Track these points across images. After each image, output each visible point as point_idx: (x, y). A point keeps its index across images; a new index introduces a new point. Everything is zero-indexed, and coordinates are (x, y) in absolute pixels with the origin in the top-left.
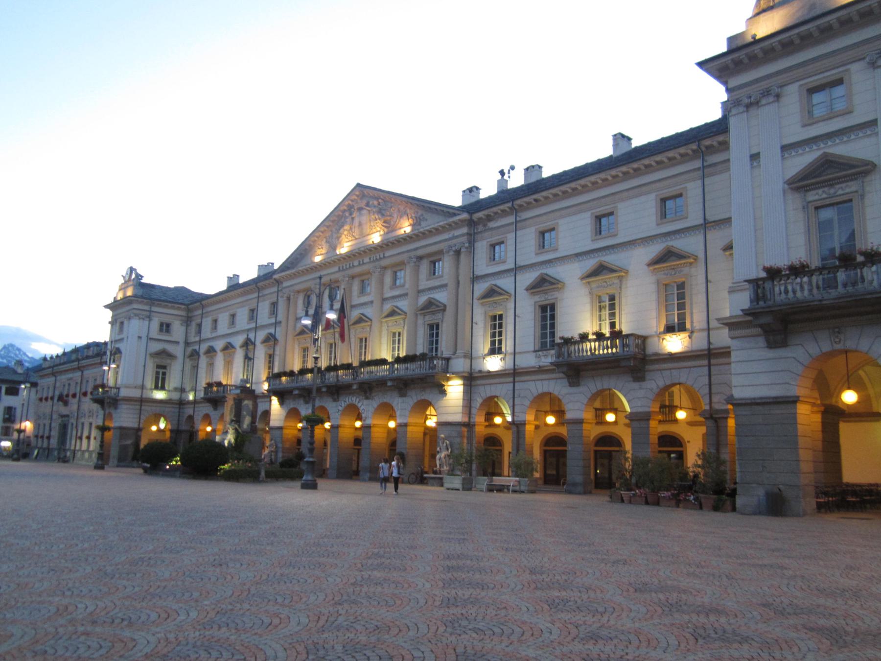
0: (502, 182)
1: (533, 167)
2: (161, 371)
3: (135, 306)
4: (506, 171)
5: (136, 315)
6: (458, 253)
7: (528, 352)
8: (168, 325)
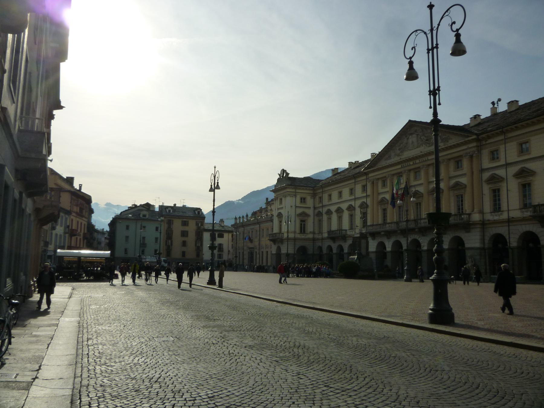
0: (494, 109)
1: (513, 101)
2: (303, 223)
3: (288, 190)
4: (496, 102)
5: (289, 195)
6: (471, 157)
7: (516, 209)
8: (304, 199)
